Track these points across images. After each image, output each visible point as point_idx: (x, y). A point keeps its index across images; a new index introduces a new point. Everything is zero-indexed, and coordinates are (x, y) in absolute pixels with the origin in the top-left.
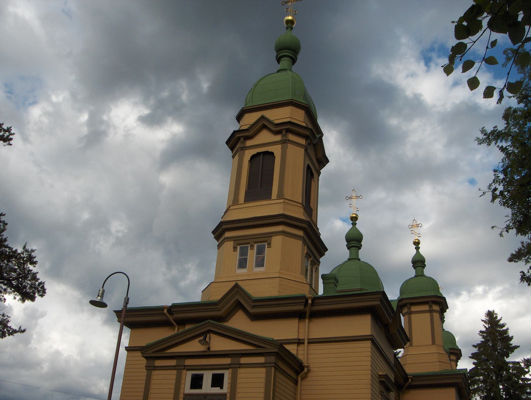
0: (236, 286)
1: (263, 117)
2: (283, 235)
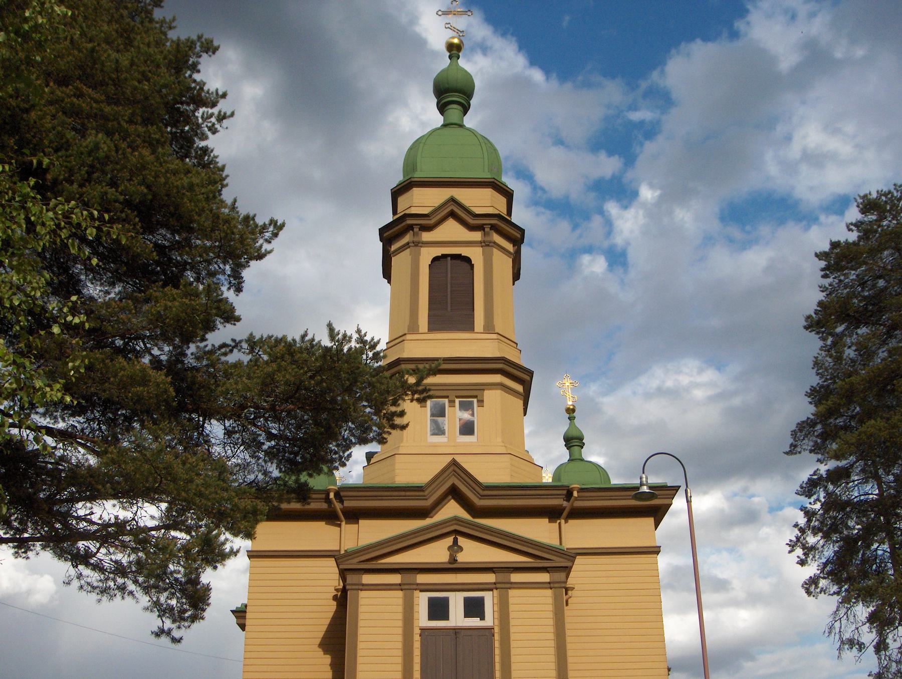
2: (502, 390)
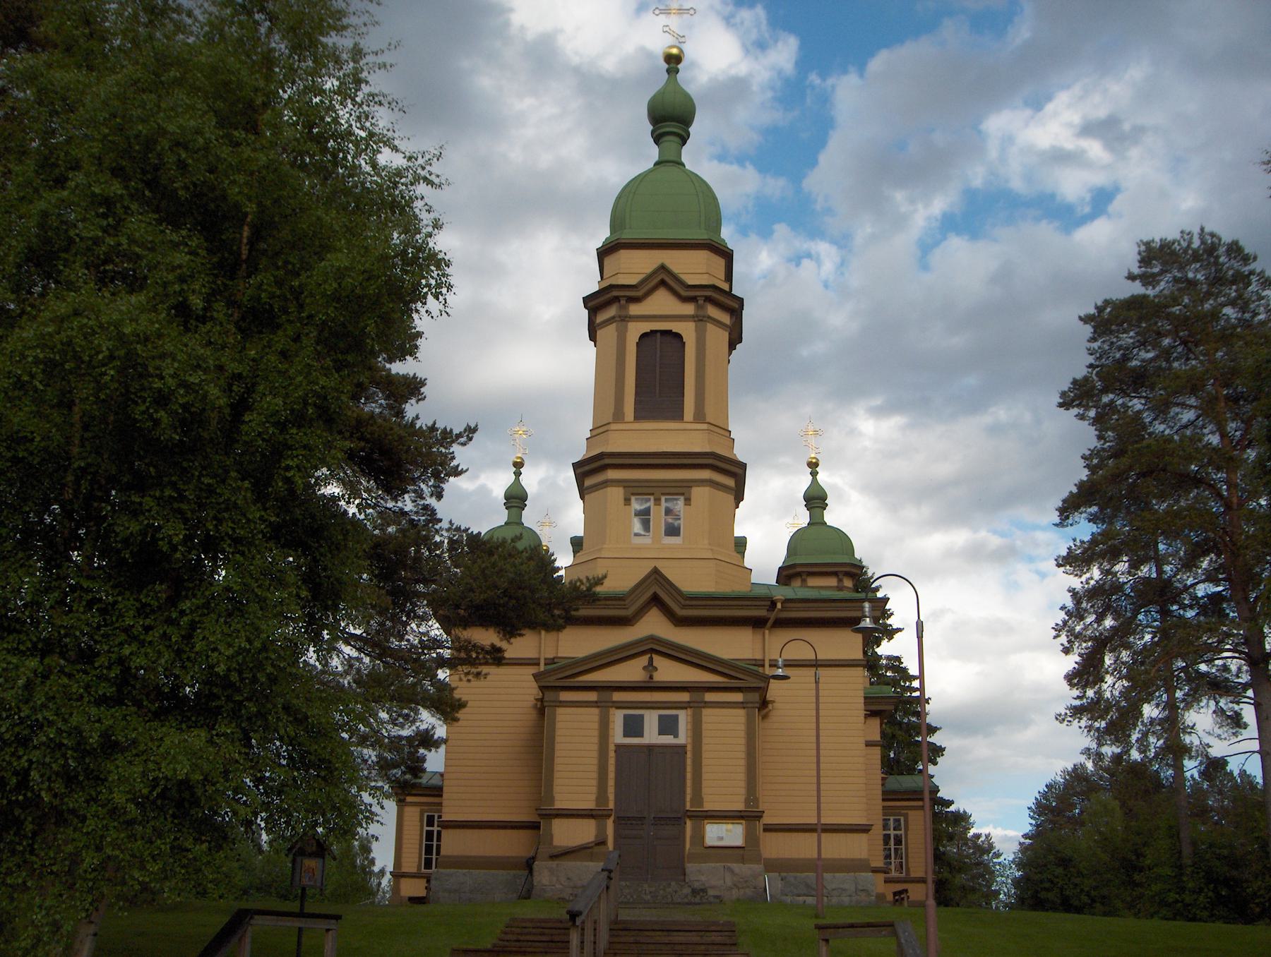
0: (656, 571)
1: (663, 268)
